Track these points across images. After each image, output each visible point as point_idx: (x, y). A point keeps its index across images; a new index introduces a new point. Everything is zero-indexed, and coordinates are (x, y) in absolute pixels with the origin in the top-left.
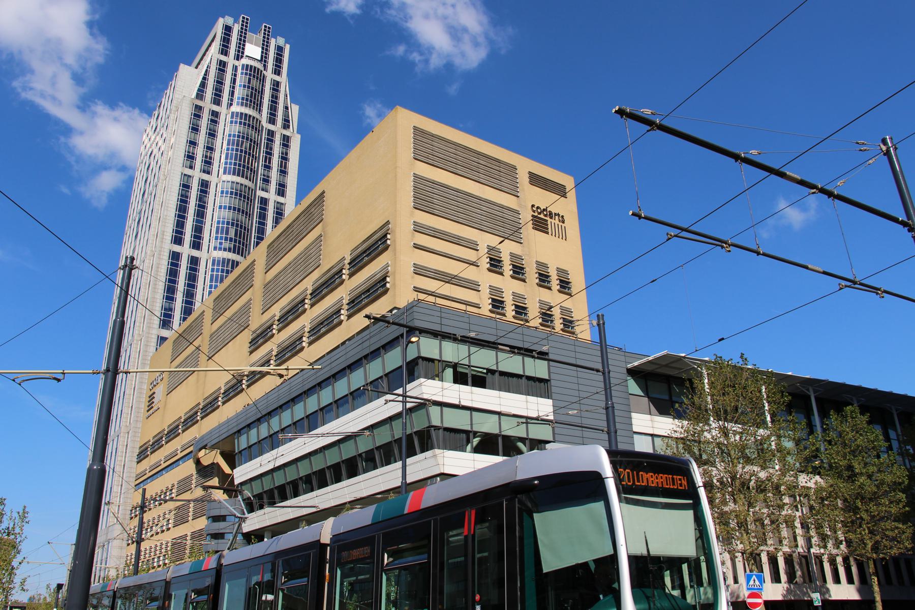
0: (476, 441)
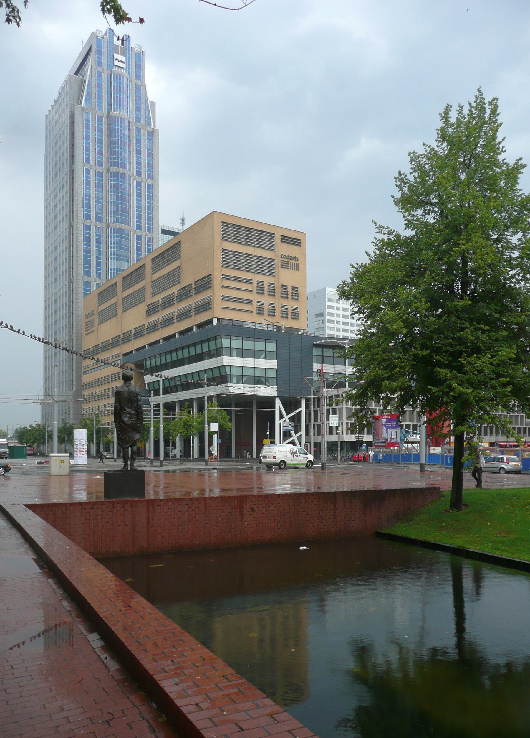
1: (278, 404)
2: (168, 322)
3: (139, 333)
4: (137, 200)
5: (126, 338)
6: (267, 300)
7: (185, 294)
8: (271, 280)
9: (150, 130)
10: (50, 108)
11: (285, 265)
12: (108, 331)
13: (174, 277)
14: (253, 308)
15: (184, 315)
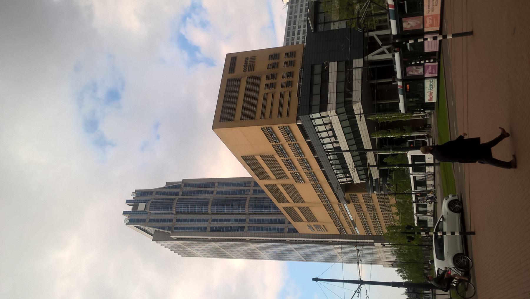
0: (348, 90)
1: (372, 57)
3: (318, 188)
5: (324, 198)
6: (280, 80)
7: (281, 150)
8: (264, 78)
10: (177, 254)
12: (321, 213)
14: (286, 90)
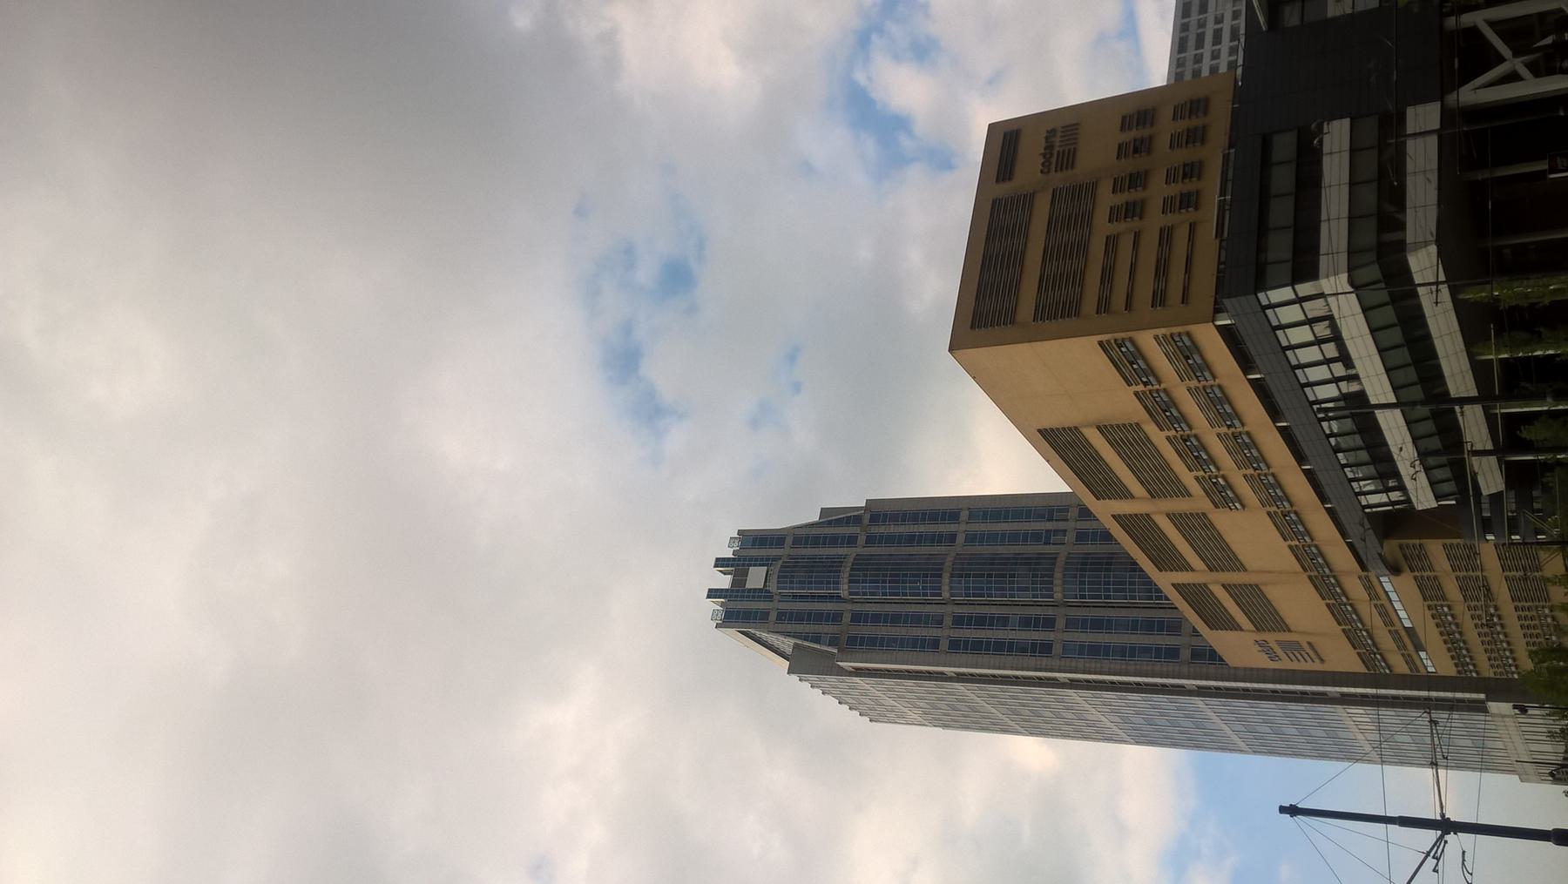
1: (1472, 94)
2: (1245, 448)
3: (1289, 524)
4: (1003, 539)
5: (1309, 558)
6: (1159, 189)
7: (1163, 409)
8: (1105, 190)
9: (868, 516)
11: (1066, 160)
12: (1300, 605)
13: (1123, 436)
14: (1180, 219)
15: (1219, 405)
